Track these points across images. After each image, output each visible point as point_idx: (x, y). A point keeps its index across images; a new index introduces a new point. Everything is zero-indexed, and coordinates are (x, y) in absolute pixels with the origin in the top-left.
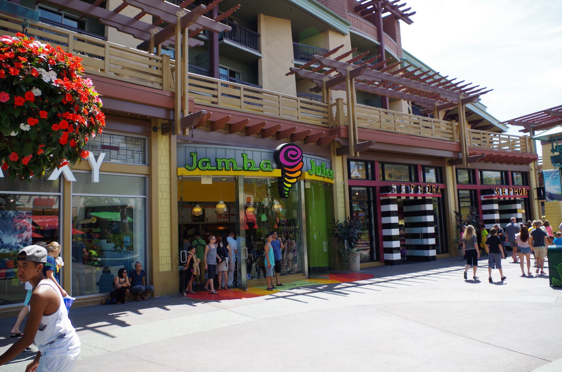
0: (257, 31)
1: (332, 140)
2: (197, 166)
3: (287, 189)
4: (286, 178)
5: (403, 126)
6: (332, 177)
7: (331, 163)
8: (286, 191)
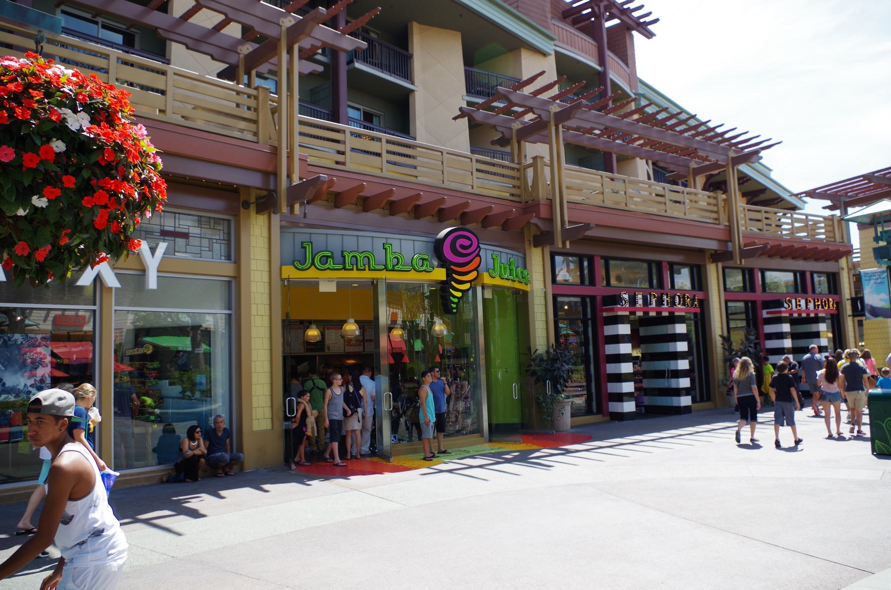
0: (407, 49)
2: (313, 263)
3: (456, 300)
4: (453, 283)
6: (526, 280)
7: (524, 259)
8: (454, 303)
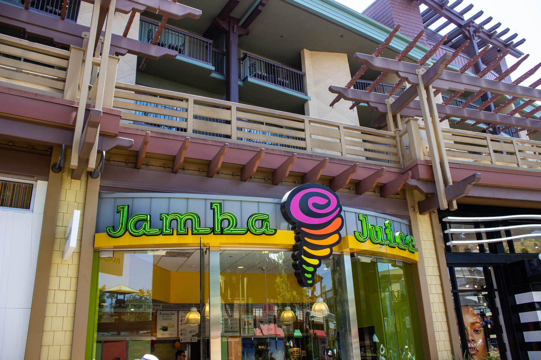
0: (301, 70)
1: (404, 191)
2: (127, 229)
3: (311, 269)
4: (305, 248)
5: (528, 152)
6: (413, 249)
7: (410, 227)
8: (308, 272)
